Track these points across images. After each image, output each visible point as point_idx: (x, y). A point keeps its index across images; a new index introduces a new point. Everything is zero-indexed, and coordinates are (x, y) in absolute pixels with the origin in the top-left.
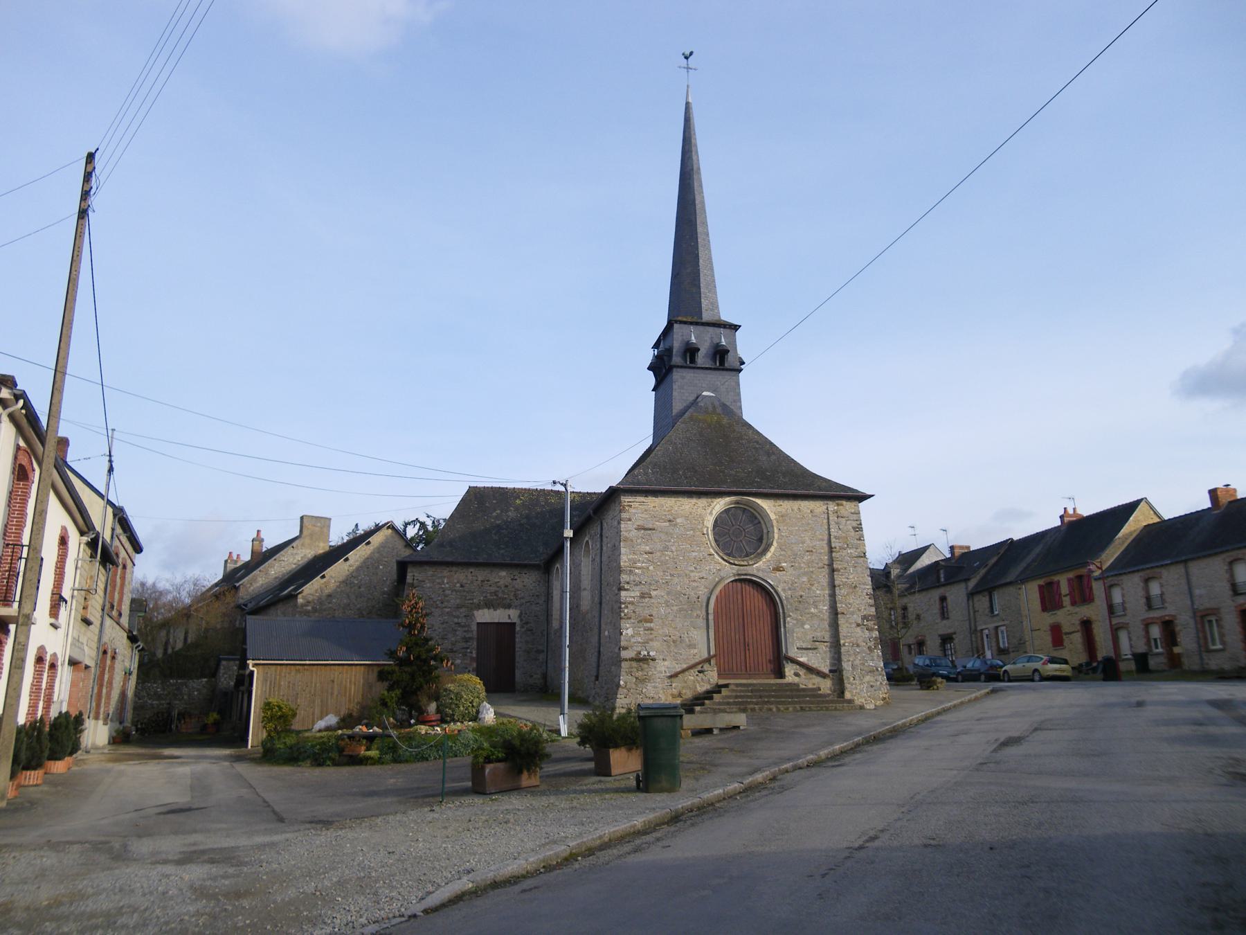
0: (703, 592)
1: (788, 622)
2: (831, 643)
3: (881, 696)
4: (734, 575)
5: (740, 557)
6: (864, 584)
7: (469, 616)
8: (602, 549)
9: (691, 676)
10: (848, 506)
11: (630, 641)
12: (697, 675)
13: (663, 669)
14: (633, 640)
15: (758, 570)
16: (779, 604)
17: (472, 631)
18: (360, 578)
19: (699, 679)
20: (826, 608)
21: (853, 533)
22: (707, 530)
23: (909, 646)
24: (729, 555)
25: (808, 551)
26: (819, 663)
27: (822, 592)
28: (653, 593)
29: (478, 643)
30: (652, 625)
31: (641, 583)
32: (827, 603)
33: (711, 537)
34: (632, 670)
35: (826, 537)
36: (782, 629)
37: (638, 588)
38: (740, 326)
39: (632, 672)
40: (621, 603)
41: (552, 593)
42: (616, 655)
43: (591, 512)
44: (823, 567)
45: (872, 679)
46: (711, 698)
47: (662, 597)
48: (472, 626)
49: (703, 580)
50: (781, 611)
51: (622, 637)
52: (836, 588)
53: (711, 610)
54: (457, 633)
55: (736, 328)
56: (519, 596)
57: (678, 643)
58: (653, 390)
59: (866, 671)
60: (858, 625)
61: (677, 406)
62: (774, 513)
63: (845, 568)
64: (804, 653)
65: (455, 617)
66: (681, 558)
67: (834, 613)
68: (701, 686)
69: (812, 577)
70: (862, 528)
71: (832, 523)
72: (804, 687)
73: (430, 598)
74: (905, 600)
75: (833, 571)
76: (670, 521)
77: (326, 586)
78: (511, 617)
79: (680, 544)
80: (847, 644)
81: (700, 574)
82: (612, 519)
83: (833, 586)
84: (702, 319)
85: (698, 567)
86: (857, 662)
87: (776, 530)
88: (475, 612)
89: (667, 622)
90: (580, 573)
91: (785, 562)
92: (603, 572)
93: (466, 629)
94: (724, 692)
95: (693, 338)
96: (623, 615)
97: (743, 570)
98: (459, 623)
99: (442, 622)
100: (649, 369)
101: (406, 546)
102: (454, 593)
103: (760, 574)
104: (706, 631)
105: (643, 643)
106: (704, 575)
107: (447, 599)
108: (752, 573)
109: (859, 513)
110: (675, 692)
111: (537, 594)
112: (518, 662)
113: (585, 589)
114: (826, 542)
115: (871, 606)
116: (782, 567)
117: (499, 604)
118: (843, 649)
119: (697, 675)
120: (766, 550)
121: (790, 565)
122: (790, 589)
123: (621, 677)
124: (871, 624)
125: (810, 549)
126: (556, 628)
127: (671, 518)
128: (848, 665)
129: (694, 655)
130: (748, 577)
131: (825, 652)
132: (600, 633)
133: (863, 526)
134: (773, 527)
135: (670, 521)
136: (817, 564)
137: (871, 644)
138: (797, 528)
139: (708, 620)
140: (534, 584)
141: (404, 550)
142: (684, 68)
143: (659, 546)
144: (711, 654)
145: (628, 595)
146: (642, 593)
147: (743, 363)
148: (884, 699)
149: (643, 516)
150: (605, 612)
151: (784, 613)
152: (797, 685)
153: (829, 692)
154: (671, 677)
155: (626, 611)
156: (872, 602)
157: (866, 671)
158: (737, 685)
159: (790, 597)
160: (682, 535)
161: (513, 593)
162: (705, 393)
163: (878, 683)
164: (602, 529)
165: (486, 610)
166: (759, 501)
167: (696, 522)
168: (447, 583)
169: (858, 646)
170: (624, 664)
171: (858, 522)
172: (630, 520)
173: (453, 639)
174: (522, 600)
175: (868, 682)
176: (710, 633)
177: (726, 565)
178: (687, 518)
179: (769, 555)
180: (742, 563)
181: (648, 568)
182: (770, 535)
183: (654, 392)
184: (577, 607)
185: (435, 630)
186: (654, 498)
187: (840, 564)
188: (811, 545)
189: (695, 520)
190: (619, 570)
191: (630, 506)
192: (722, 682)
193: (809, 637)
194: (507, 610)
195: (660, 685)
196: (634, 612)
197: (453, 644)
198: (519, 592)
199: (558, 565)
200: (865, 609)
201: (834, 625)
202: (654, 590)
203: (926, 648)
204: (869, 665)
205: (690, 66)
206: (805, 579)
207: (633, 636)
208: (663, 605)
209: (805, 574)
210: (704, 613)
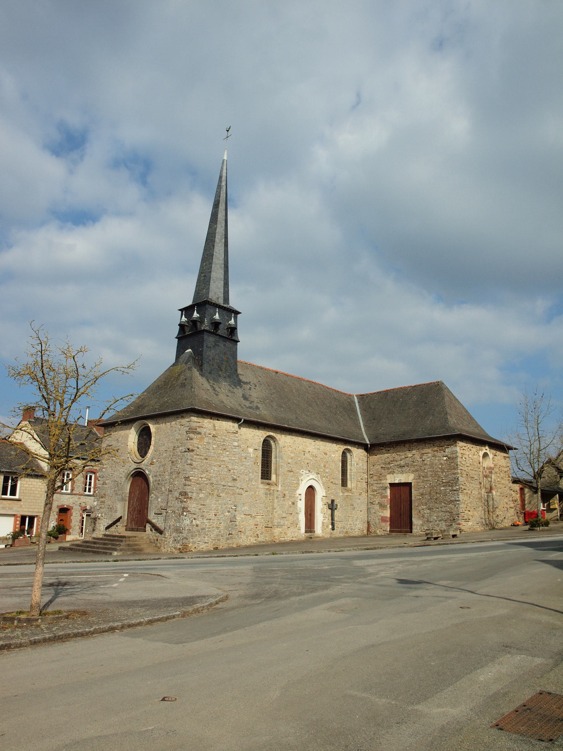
38: (241, 313)
45: (177, 535)
55: (239, 313)
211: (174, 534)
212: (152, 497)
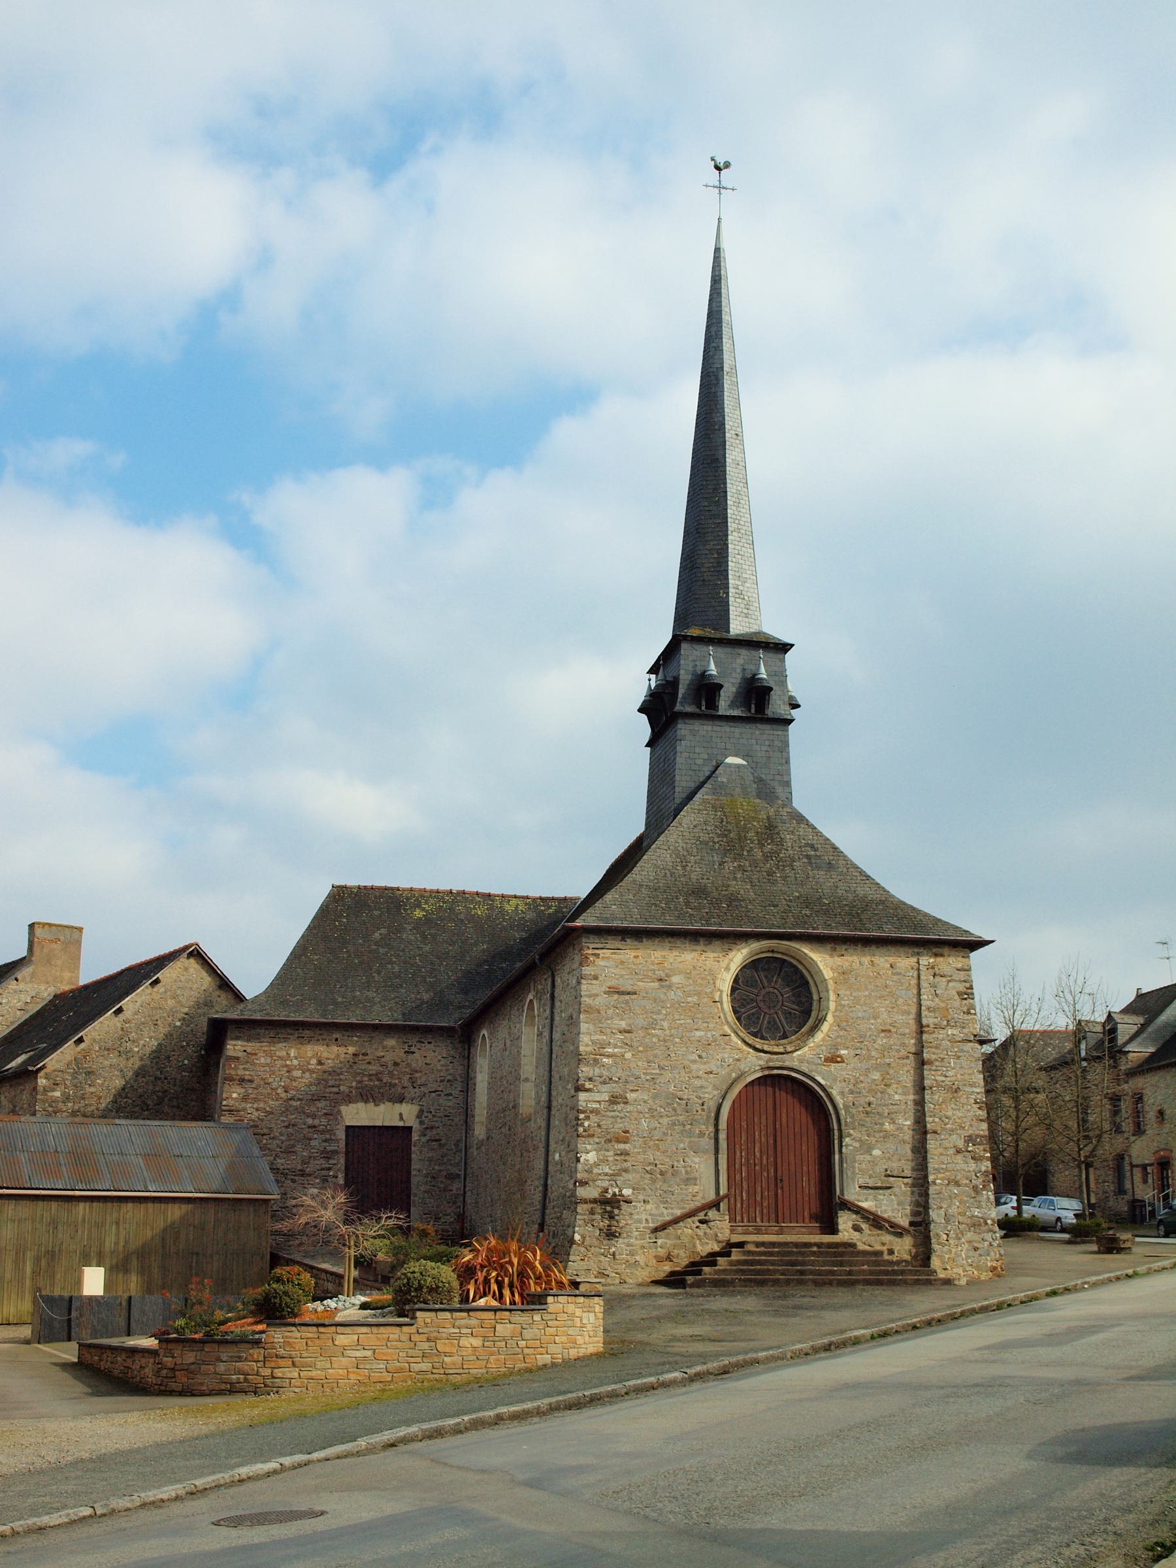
0: (711, 1095)
3: (989, 1264)
4: (763, 1069)
5: (774, 1039)
6: (971, 1086)
7: (333, 1115)
8: (552, 1020)
9: (687, 1229)
10: (950, 962)
11: (591, 1172)
12: (697, 1227)
15: (801, 1061)
16: (834, 1116)
17: (338, 1141)
18: (142, 1042)
19: (700, 1232)
20: (908, 1123)
21: (957, 1002)
22: (721, 997)
23: (1144, 1167)
24: (755, 1035)
25: (883, 1031)
26: (893, 1211)
27: (902, 1096)
28: (631, 1096)
29: (347, 1161)
30: (627, 1147)
32: (911, 1114)
33: (727, 1005)
34: (594, 1217)
35: (914, 1010)
36: (837, 1157)
38: (792, 645)
41: (475, 1077)
43: (537, 957)
44: (908, 1057)
45: (976, 1237)
46: (714, 1264)
47: (645, 1102)
48: (337, 1132)
49: (711, 1076)
50: (836, 1127)
51: (579, 1166)
52: (926, 1092)
53: (723, 1125)
54: (313, 1143)
55: (785, 648)
56: (419, 1082)
57: (669, 1175)
58: (646, 746)
60: (958, 1152)
61: (683, 781)
62: (832, 969)
63: (943, 1059)
66: (677, 1040)
68: (702, 1244)
69: (888, 1074)
70: (973, 994)
71: (924, 984)
74: (1140, 1082)
75: (921, 1063)
76: (661, 980)
77: (85, 1057)
79: (677, 1017)
80: (938, 1181)
81: (706, 1066)
82: (569, 973)
83: (921, 1088)
85: (704, 1055)
86: (953, 1210)
87: (832, 996)
88: (343, 1108)
89: (652, 1143)
90: (519, 1053)
92: (554, 1056)
93: (328, 1136)
95: (712, 666)
96: (581, 1129)
97: (776, 1061)
98: (315, 1127)
99: (286, 1124)
101: (220, 987)
102: (307, 1075)
105: (611, 1175)
106: (714, 1069)
107: (294, 1084)
110: (662, 1252)
112: (415, 1195)
113: (527, 1080)
114: (913, 1016)
115: (981, 1120)
118: (932, 1190)
119: (697, 1227)
121: (853, 1053)
122: (851, 1092)
123: (577, 1229)
124: (979, 1150)
125: (888, 1027)
126: (481, 1137)
127: (663, 975)
129: (694, 1196)
130: (785, 1072)
133: (975, 991)
134: (828, 991)
135: (661, 980)
136: (898, 1051)
137: (979, 1182)
138: (867, 993)
142: (714, 187)
144: (721, 1193)
145: (590, 1099)
147: (796, 706)
148: (994, 1269)
149: (617, 971)
150: (555, 1122)
151: (840, 1130)
152: (853, 1245)
153: (907, 1257)
154: (656, 1230)
155: (586, 1124)
156: (983, 1114)
158: (758, 1244)
159: (851, 1104)
161: (408, 1076)
162: (731, 760)
163: (986, 1244)
165: (361, 1105)
168: (296, 1058)
169: (957, 1184)
171: (968, 985)
172: (596, 978)
173: (305, 1154)
174: (422, 1089)
178: (688, 976)
179: (819, 1036)
180: (776, 1049)
181: (623, 1056)
183: (649, 748)
184: (514, 1107)
185: (274, 1138)
186: (636, 943)
188: (889, 1021)
191: (597, 955)
192: (735, 1239)
193: (880, 1169)
195: (638, 1242)
196: (599, 1126)
197: (304, 1163)
198: (418, 1075)
201: (920, 1151)
202: (632, 1091)
203: (1172, 1173)
204: (973, 1216)
205: (724, 184)
206: (876, 1076)
207: (596, 1165)
209: (877, 1067)
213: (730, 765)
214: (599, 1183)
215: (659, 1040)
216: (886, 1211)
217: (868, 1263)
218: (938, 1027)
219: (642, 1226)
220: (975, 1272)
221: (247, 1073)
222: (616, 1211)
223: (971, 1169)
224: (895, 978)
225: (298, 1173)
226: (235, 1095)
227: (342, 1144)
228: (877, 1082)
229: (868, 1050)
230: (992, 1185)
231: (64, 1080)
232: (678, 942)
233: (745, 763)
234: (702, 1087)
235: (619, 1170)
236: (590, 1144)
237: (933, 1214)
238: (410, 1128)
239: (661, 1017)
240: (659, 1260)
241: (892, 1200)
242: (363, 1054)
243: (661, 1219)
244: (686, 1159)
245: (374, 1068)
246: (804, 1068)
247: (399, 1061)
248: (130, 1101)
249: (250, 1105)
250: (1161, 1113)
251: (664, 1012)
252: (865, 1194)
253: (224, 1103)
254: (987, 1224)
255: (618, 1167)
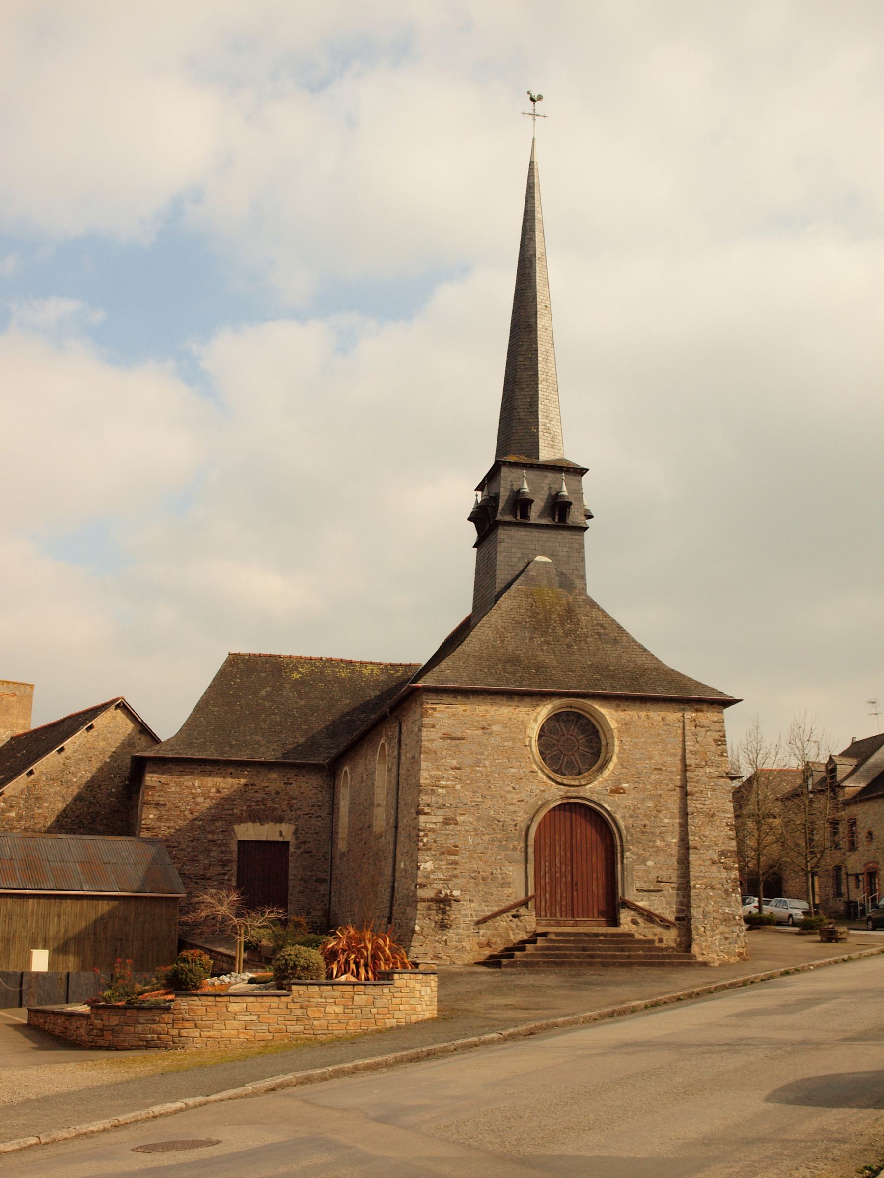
0: (522, 818)
1: (627, 858)
2: (679, 884)
3: (737, 951)
4: (562, 798)
5: (571, 775)
6: (724, 812)
7: (228, 832)
9: (503, 922)
10: (708, 716)
12: (511, 921)
13: (469, 912)
14: (432, 876)
15: (592, 792)
16: (617, 835)
17: (231, 852)
18: (79, 774)
19: (513, 925)
21: (713, 747)
22: (530, 741)
24: (556, 771)
25: (656, 769)
27: (670, 820)
28: (460, 819)
29: (239, 867)
30: (457, 858)
31: (444, 805)
32: (677, 834)
33: (535, 749)
36: (619, 866)
37: (440, 812)
38: (588, 470)
39: (430, 915)
40: (419, 830)
42: (411, 894)
43: (388, 710)
44: (675, 790)
45: (727, 930)
49: (523, 803)
50: (618, 843)
51: (420, 873)
52: (689, 817)
53: (531, 841)
54: (212, 854)
55: (582, 471)
57: (489, 880)
59: (720, 920)
60: (714, 863)
61: (502, 575)
63: (702, 791)
64: (644, 896)
65: (209, 832)
67: (685, 846)
68: (514, 934)
69: (659, 802)
71: (687, 733)
72: (643, 937)
73: (176, 807)
74: (853, 810)
76: (484, 728)
77: (34, 786)
78: (284, 834)
79: (496, 757)
80: (698, 886)
81: (518, 796)
83: (684, 814)
84: (538, 458)
85: (517, 787)
86: (710, 908)
87: (617, 742)
88: (236, 827)
90: (373, 784)
91: (627, 782)
92: (400, 787)
93: (224, 849)
94: (541, 942)
96: (421, 844)
97: (573, 792)
98: (214, 841)
99: (191, 839)
100: (470, 519)
103: (595, 798)
104: (523, 866)
106: (525, 797)
108: (584, 796)
109: (723, 722)
110: (483, 940)
111: (319, 803)
113: (379, 805)
114: (679, 758)
115: (732, 839)
116: (622, 789)
117: (267, 817)
118: (693, 893)
119: (511, 921)
120: (607, 761)
121: (632, 786)
122: (631, 816)
123: (417, 921)
124: (729, 862)
127: (485, 725)
128: (698, 913)
129: (508, 896)
130: (580, 801)
131: (672, 895)
132: (395, 864)
133: (727, 739)
134: (613, 738)
135: (484, 728)
136: (667, 785)
137: (729, 887)
138: (643, 740)
139: (526, 853)
140: (314, 791)
141: (139, 736)
143: (469, 760)
144: (530, 894)
145: (428, 821)
146: (446, 819)
147: (590, 517)
148: (740, 954)
149: (450, 721)
150: (401, 838)
151: (622, 846)
153: (673, 945)
154: (478, 923)
155: (425, 840)
156: (733, 834)
157: (720, 920)
160: (498, 746)
162: (539, 558)
163: (735, 935)
164: (400, 733)
165: (250, 824)
166: (589, 702)
167: (516, 730)
168: (199, 787)
169: (712, 888)
170: (420, 906)
171: (721, 734)
172: (433, 726)
173: (206, 862)
174: (298, 812)
175: (722, 933)
176: (529, 869)
177: (552, 786)
178: (505, 725)
179: (606, 773)
180: (573, 783)
181: (454, 787)
182: (610, 747)
184: (369, 827)
186: (465, 700)
187: (695, 787)
189: (516, 728)
190: (419, 789)
191: (435, 709)
192: (540, 930)
193: (653, 876)
194: (278, 825)
195: (465, 932)
198: (294, 801)
199: (346, 768)
200: (723, 843)
201: (684, 863)
202: (461, 814)
203: (879, 880)
204: (725, 913)
205: (537, 112)
206: (650, 804)
207: (433, 872)
208: (472, 834)
209: (651, 797)
210: (522, 844)
211: (722, 928)
212: (627, 858)
213: (539, 562)
214: (435, 886)
215: (482, 775)
216: (657, 909)
217: (643, 949)
218: (698, 766)
219: (468, 919)
220: (726, 957)
221: (162, 799)
222: (448, 908)
223: (723, 877)
224: (666, 728)
225: (200, 877)
226: (151, 816)
227: (235, 854)
228: (651, 809)
229: (644, 784)
230: (739, 889)
231: (18, 803)
232: (498, 699)
233: (550, 560)
234: (515, 812)
235: (450, 876)
236: (428, 856)
237: (694, 912)
238: (288, 843)
239: (483, 757)
240: (481, 946)
241: (662, 901)
242: (252, 785)
243: (482, 914)
244: (503, 868)
245: (261, 795)
246: (595, 798)
247: (280, 790)
248: (69, 820)
249: (163, 824)
250: (870, 834)
251: (486, 754)
252: (641, 896)
253: (143, 822)
254: (735, 919)
255: (450, 874)
